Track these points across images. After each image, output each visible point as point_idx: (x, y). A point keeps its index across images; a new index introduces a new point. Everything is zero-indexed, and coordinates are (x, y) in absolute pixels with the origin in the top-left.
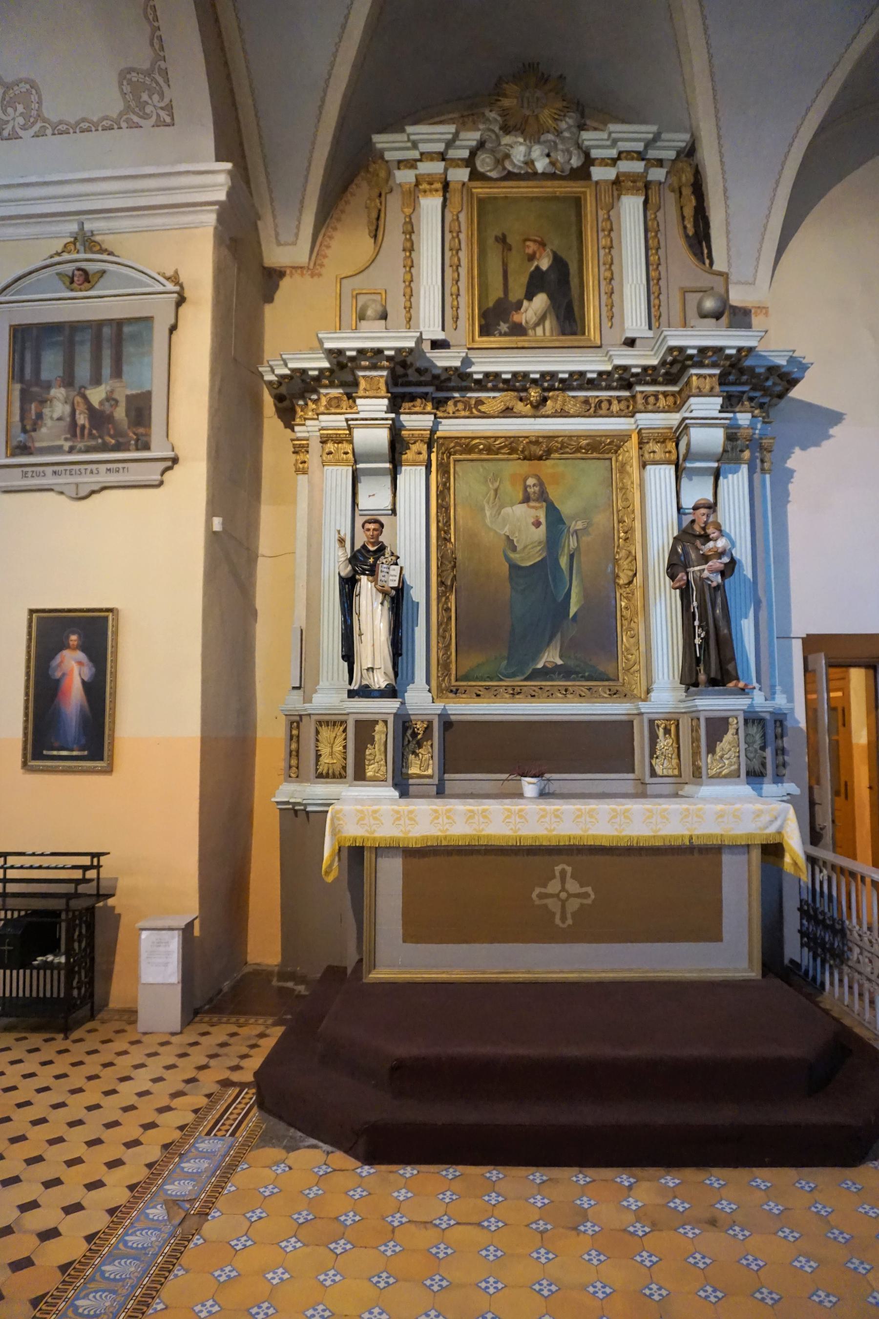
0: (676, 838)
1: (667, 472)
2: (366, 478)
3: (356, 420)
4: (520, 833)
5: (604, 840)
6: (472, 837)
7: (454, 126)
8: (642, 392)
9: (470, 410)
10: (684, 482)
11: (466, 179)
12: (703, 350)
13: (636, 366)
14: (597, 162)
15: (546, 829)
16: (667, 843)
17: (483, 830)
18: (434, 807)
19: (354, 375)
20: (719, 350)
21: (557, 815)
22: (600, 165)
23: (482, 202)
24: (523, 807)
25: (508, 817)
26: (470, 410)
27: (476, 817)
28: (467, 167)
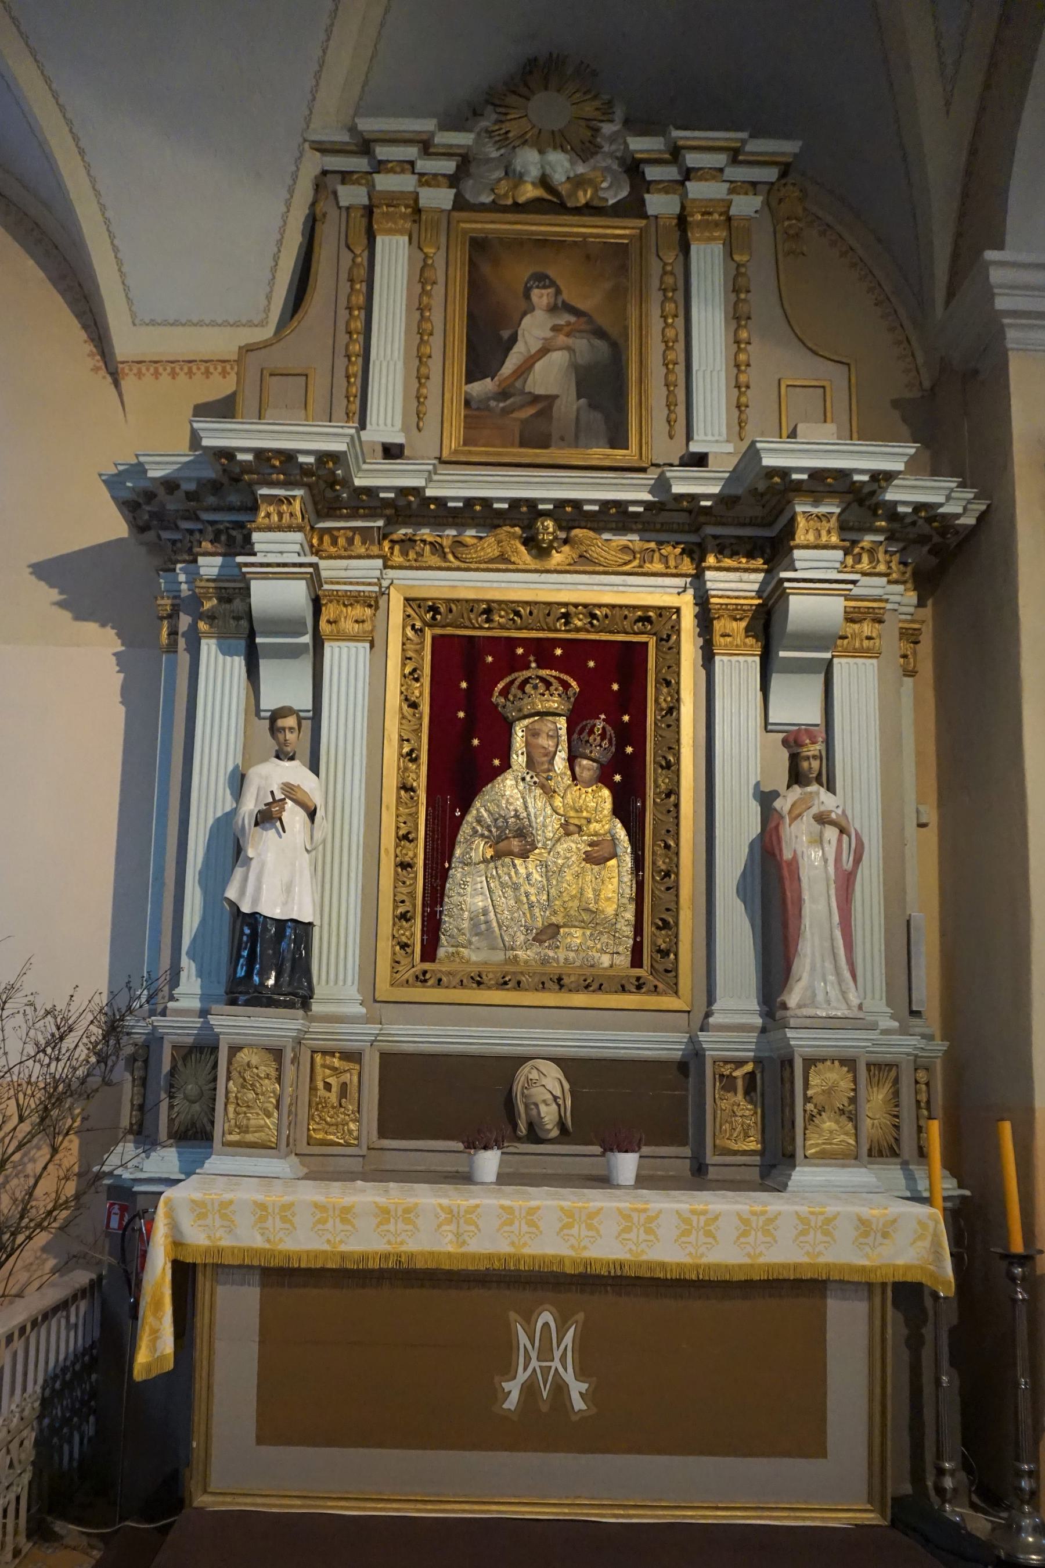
0: (784, 1266)
1: (353, 650)
2: (779, 675)
3: (253, 565)
4: (587, 1254)
5: (304, 1258)
6: (505, 1258)
7: (800, 143)
8: (715, 537)
9: (444, 557)
10: (777, 681)
11: (448, 206)
12: (817, 475)
13: (905, 503)
14: (652, 187)
15: (808, 1253)
16: (497, 1265)
17: (702, 1255)
18: (445, 1202)
19: (254, 494)
20: (843, 474)
21: (345, 1214)
22: (659, 191)
23: (479, 246)
24: (477, 1201)
25: (803, 1233)
26: (444, 557)
27: (812, 1232)
28: (451, 187)
